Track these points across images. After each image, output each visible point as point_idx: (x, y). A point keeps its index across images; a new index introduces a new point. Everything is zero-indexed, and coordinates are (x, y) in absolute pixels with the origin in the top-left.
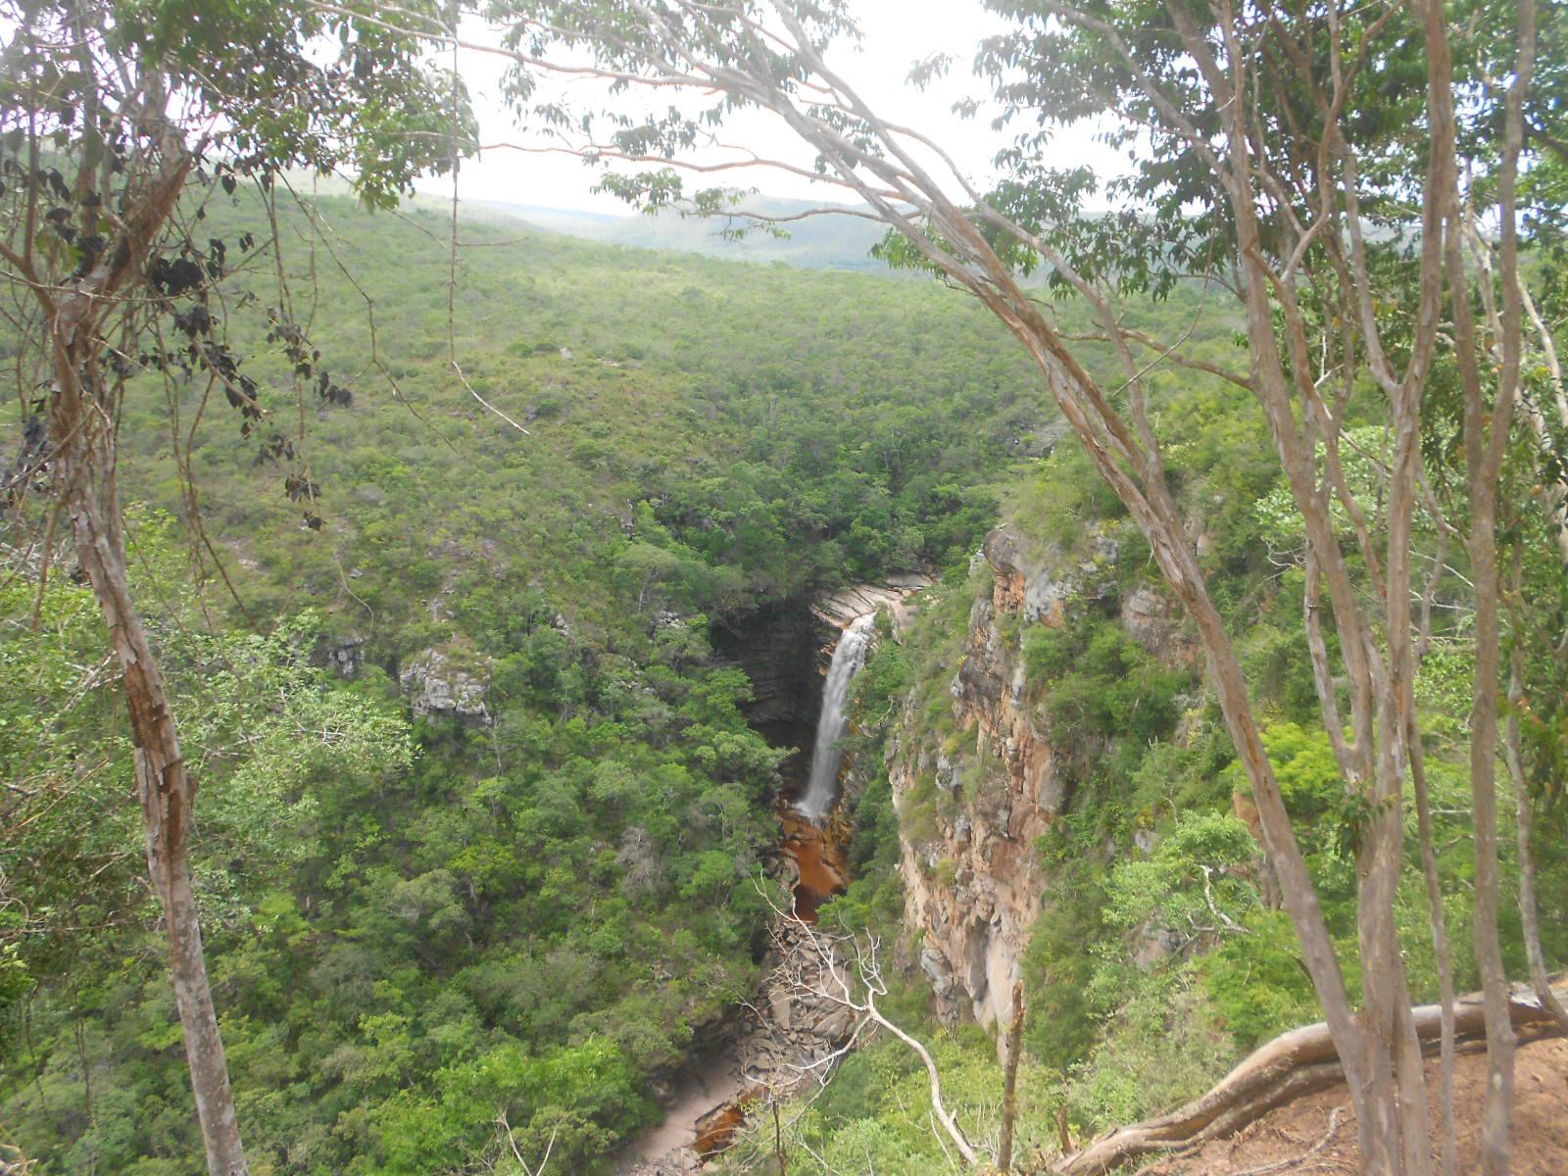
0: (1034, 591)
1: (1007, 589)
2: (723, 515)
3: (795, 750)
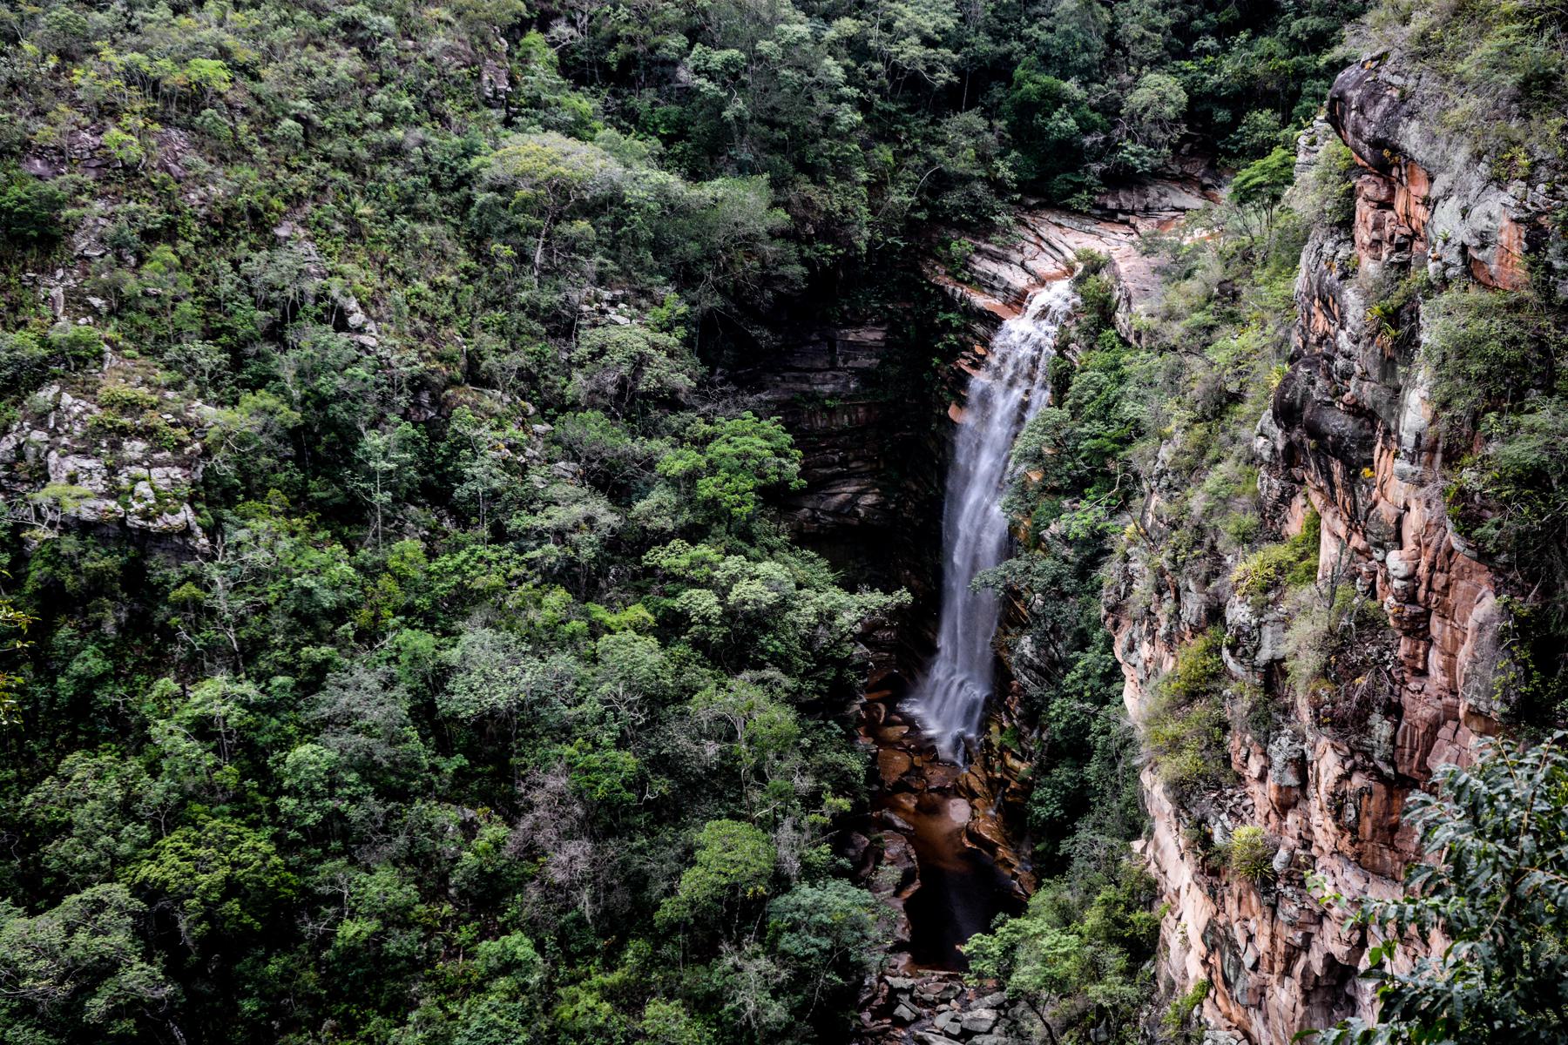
0: (1454, 204)
1: (1386, 205)
2: (718, 57)
3: (904, 596)
